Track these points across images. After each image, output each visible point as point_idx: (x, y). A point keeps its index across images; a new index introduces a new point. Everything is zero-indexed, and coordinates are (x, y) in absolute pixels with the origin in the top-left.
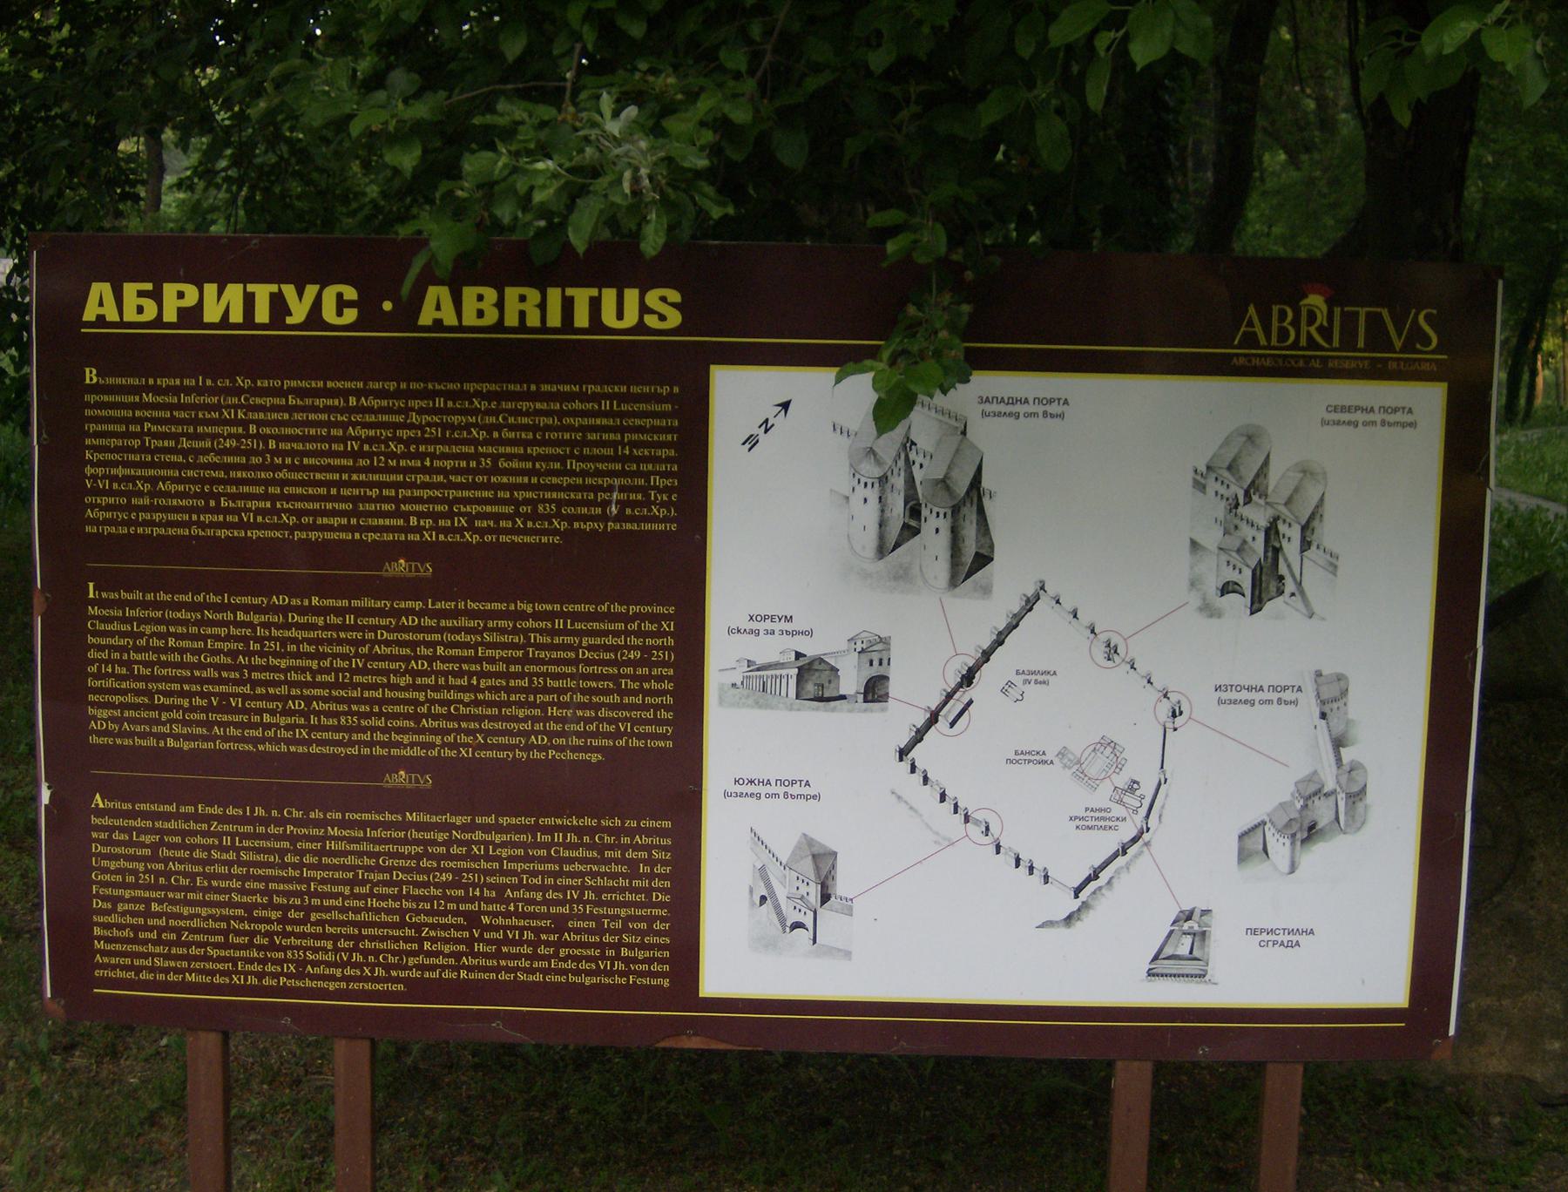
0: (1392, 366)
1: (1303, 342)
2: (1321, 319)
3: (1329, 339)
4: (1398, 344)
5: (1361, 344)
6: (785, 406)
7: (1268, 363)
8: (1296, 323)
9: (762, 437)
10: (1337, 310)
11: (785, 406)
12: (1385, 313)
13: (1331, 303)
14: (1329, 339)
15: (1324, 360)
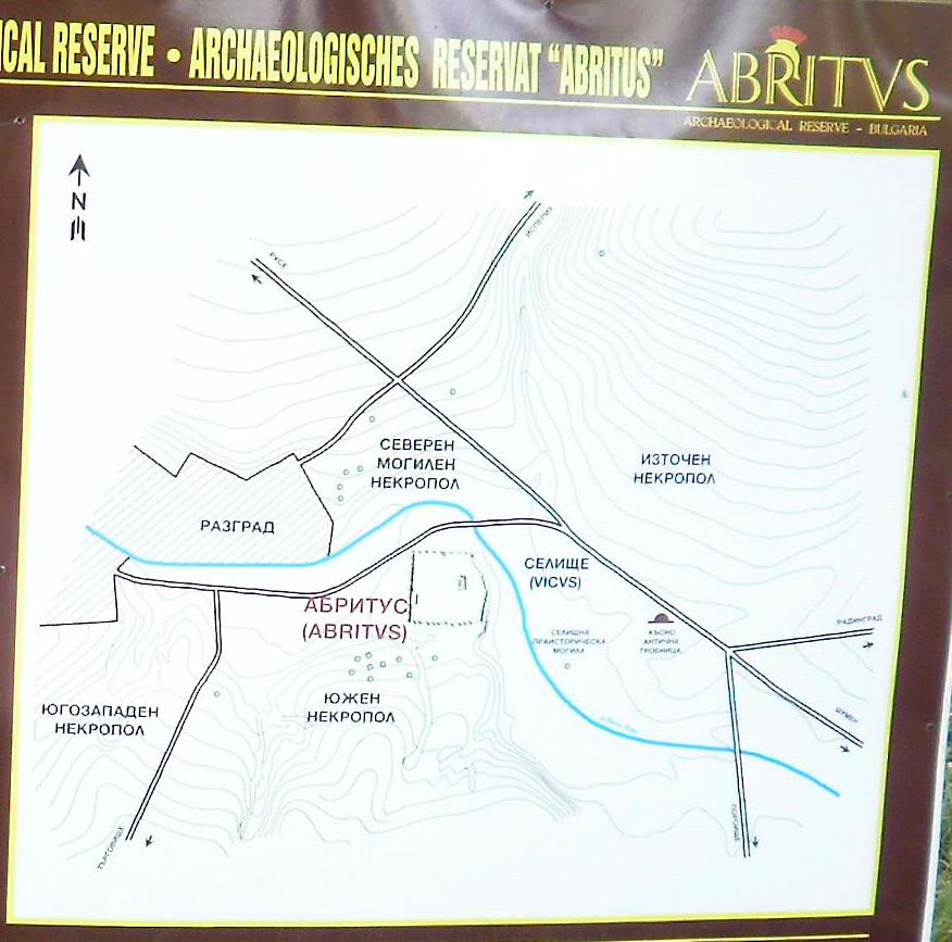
0: (874, 129)
1: (770, 100)
2: (791, 71)
3: (800, 96)
4: (881, 103)
5: (838, 103)
6: (79, 165)
7: (913, 131)
8: (761, 75)
9: (84, 215)
10: (811, 59)
11: (79, 165)
12: (866, 63)
13: (803, 51)
14: (800, 96)
15: (794, 121)
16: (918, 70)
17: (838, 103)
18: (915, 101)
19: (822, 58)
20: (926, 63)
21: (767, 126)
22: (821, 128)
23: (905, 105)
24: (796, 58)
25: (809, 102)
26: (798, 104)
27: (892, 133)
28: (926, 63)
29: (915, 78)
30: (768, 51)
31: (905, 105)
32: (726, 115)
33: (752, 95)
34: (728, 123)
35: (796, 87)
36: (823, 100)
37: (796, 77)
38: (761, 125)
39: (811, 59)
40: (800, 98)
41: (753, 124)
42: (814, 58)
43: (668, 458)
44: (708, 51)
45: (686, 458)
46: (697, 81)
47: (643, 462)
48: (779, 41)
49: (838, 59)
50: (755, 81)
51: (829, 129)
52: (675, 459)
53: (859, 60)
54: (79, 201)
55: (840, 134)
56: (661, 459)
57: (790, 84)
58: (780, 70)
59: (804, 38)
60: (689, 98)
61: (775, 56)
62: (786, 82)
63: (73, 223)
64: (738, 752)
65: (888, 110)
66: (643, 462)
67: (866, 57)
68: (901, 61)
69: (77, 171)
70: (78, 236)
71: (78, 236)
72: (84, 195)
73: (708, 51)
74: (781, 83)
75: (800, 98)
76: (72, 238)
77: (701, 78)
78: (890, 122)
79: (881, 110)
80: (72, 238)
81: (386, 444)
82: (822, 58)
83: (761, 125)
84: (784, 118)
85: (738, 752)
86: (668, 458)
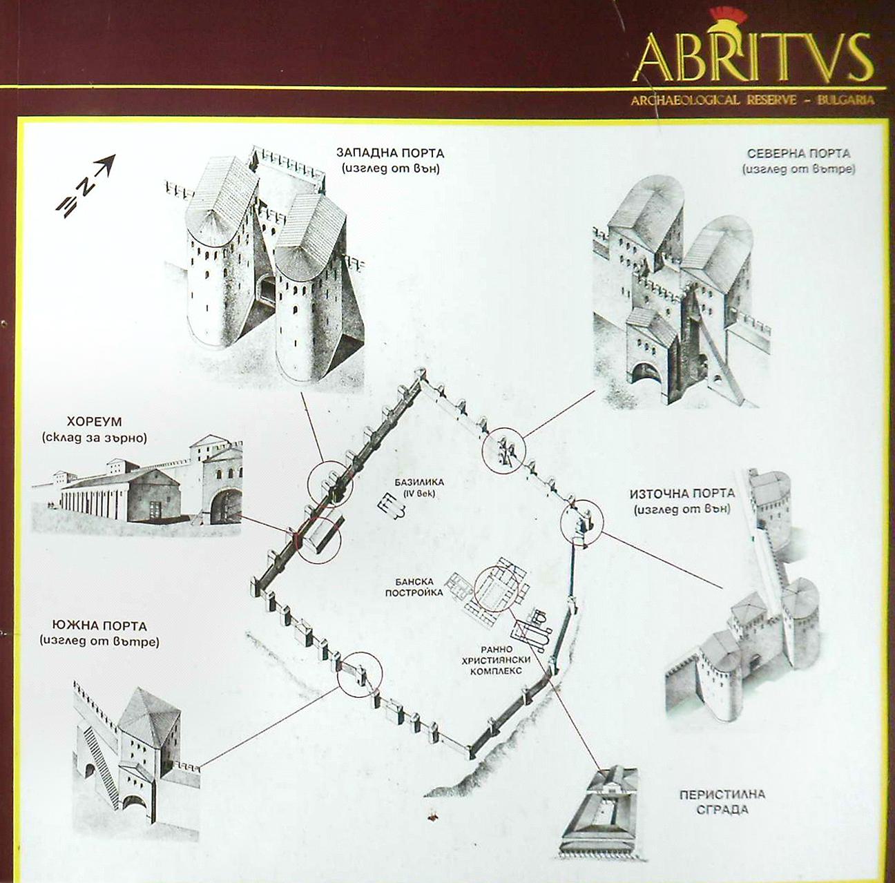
0: (822, 100)
1: (715, 76)
2: (735, 48)
4: (827, 75)
5: (784, 76)
6: (108, 162)
7: (861, 101)
8: (705, 53)
10: (753, 37)
11: (108, 162)
12: (809, 38)
13: (745, 29)
15: (742, 96)
16: (860, 42)
17: (784, 76)
18: (860, 71)
19: (763, 35)
20: (867, 36)
21: (715, 101)
22: (769, 101)
23: (851, 77)
24: (738, 35)
25: (754, 76)
26: (745, 80)
27: (840, 102)
28: (867, 36)
29: (856, 48)
30: (709, 31)
31: (851, 77)
32: (672, 93)
33: (696, 76)
34: (675, 101)
35: (741, 63)
36: (768, 74)
37: (740, 54)
38: (709, 100)
39: (753, 37)
40: (746, 73)
41: (700, 100)
42: (756, 35)
43: (652, 493)
44: (651, 34)
45: (667, 492)
46: (643, 63)
47: (632, 497)
48: (720, 21)
49: (780, 35)
50: (700, 61)
51: (776, 102)
52: (658, 494)
53: (801, 35)
54: (86, 187)
55: (788, 105)
56: (647, 494)
57: (734, 60)
58: (723, 47)
59: (745, 17)
60: (635, 79)
61: (716, 35)
62: (730, 59)
63: (70, 198)
64: (325, 519)
65: (838, 79)
66: (632, 497)
67: (808, 33)
68: (843, 35)
69: (103, 165)
70: (63, 211)
71: (63, 211)
72: (94, 185)
73: (651, 34)
74: (725, 60)
75: (746, 73)
76: (58, 209)
77: (645, 61)
78: (837, 93)
79: (828, 81)
80: (58, 209)
81: (752, 154)
82: (763, 35)
83: (709, 100)
84: (732, 93)
85: (325, 519)
86: (652, 493)
